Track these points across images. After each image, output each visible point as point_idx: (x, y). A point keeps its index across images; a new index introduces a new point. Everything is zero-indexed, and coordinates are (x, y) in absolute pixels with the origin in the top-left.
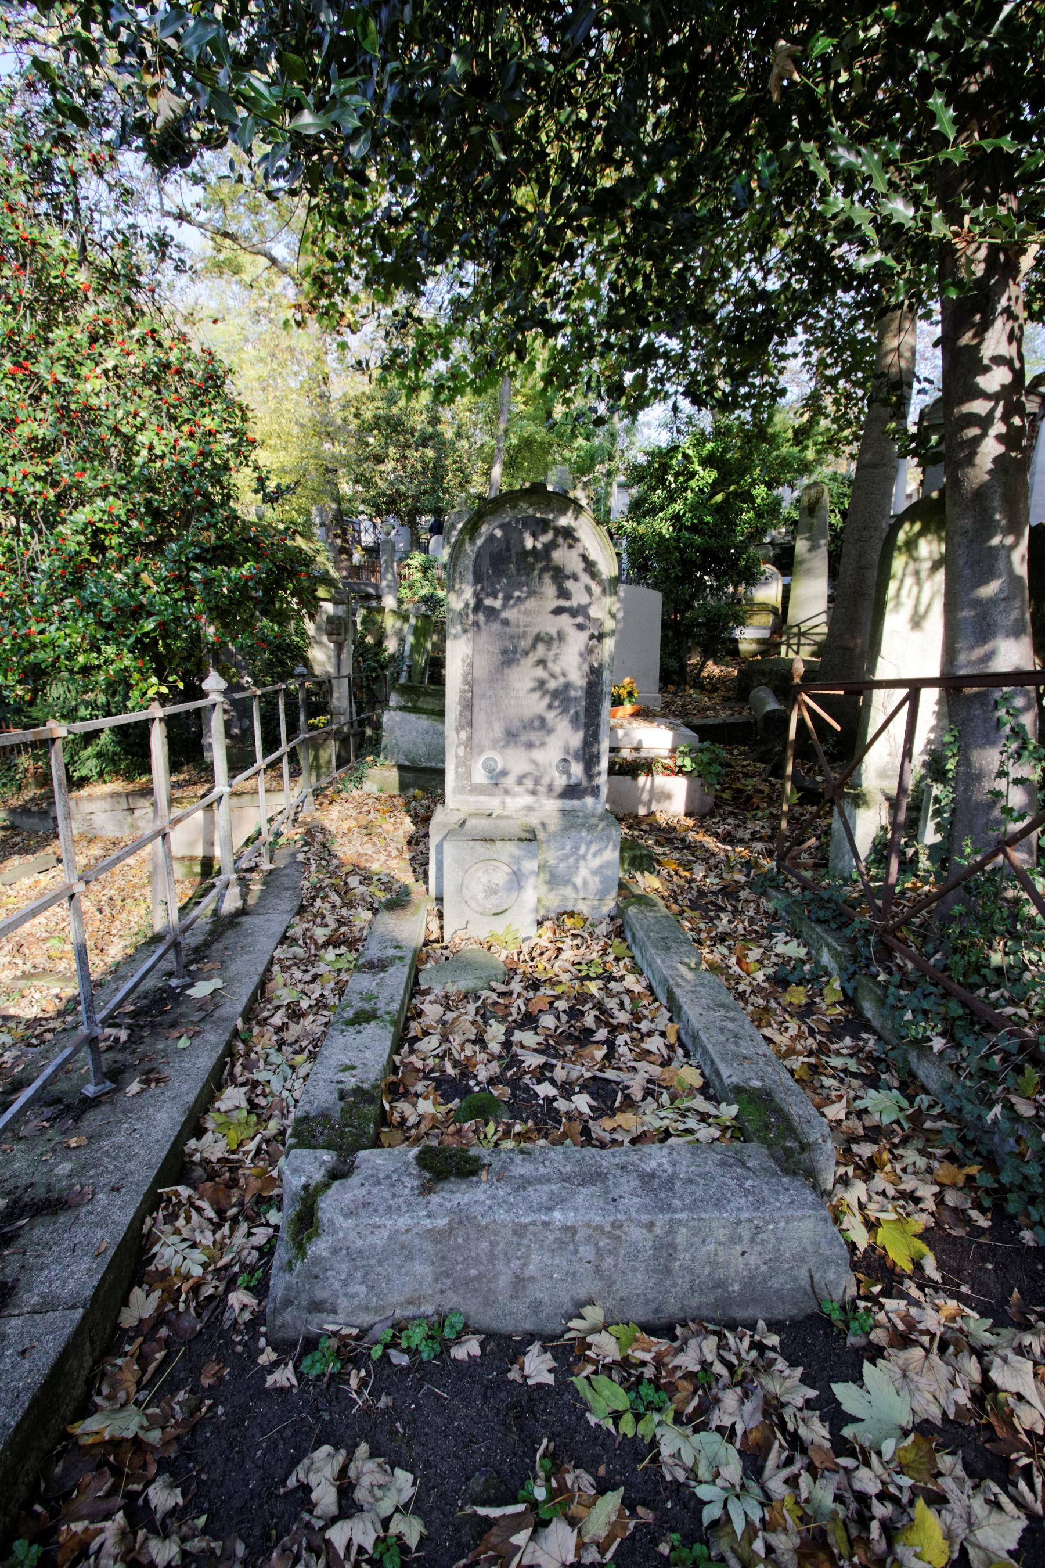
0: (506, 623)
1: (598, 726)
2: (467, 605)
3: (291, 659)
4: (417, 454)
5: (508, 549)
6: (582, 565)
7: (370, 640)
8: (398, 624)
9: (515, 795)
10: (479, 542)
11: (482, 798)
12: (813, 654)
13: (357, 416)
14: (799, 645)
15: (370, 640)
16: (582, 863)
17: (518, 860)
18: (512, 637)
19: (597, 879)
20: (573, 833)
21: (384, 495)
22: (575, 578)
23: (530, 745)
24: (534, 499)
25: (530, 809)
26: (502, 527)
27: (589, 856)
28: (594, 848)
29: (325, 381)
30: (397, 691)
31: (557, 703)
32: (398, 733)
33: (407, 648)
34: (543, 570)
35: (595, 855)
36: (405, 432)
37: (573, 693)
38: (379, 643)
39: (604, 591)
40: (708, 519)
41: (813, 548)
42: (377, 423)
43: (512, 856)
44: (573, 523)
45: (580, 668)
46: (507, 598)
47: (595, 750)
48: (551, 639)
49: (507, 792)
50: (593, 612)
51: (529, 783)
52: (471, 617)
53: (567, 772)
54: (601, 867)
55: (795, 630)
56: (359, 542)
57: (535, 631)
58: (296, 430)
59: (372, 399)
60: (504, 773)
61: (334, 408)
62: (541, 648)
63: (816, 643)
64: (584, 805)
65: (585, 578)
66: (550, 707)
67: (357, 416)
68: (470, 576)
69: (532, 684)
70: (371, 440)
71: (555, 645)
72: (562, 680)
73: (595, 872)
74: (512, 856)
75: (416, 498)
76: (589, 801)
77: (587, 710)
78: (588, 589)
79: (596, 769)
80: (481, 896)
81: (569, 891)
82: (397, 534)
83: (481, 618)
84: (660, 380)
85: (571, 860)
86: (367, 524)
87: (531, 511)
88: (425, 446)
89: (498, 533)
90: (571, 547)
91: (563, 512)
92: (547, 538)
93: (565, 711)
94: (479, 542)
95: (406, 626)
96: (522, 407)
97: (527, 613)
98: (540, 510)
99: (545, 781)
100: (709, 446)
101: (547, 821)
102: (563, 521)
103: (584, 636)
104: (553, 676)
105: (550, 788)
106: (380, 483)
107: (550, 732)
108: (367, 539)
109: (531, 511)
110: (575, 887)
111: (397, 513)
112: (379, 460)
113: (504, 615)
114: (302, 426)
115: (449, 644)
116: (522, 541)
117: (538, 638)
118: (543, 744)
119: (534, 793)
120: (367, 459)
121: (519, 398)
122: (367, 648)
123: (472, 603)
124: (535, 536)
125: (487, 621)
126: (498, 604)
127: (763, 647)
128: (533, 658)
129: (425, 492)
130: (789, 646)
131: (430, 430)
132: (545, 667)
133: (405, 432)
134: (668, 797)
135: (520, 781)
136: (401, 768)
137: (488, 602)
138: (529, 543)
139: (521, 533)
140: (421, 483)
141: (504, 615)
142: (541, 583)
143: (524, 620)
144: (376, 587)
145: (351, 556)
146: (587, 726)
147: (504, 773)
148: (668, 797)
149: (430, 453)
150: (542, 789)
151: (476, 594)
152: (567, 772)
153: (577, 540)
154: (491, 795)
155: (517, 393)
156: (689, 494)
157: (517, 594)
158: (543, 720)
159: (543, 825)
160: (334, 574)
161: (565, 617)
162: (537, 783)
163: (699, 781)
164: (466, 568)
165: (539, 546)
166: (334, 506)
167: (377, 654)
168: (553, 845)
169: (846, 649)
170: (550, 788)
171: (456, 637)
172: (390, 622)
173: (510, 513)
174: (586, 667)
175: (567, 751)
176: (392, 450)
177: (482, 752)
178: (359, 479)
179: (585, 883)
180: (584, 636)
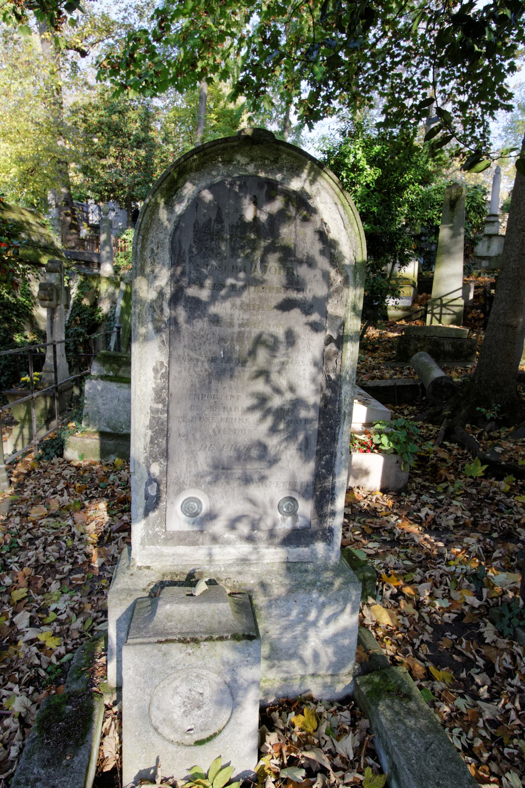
0: (216, 320)
1: (333, 455)
2: (161, 294)
3: (17, 316)
4: (133, 154)
5: (219, 220)
6: (319, 246)
7: (86, 302)
8: (111, 289)
9: (228, 543)
10: (179, 209)
11: (182, 549)
12: (453, 322)
13: (85, 121)
14: (441, 314)
15: (86, 302)
16: (311, 633)
17: (233, 669)
18: (222, 340)
19: (330, 650)
20: (301, 595)
21: (106, 184)
22: (311, 263)
23: (247, 480)
24: (257, 152)
25: (244, 561)
26: (211, 188)
27: (321, 623)
28: (328, 612)
29: (59, 90)
30: (99, 360)
31: (282, 426)
32: (100, 401)
33: (118, 310)
34: (268, 250)
35: (328, 622)
36: (124, 135)
37: (303, 414)
38: (95, 304)
39: (346, 282)
40: (375, 209)
41: (454, 236)
42: (99, 128)
43: (225, 663)
44: (308, 188)
45: (314, 380)
46: (218, 286)
47: (328, 484)
48: (276, 339)
49: (215, 539)
50: (332, 308)
51: (244, 528)
52: (167, 311)
53: (293, 513)
54: (336, 635)
55: (439, 302)
56: (87, 220)
57: (255, 332)
58: (31, 127)
59: (97, 108)
60: (211, 516)
61: (66, 114)
62: (262, 354)
63: (455, 313)
64: (314, 553)
65: (323, 263)
66: (273, 430)
67: (85, 121)
68: (166, 255)
69: (250, 402)
70: (96, 140)
71: (282, 349)
72: (289, 396)
73: (327, 642)
74: (225, 663)
75: (132, 188)
76: (320, 547)
77: (319, 433)
78: (326, 276)
79: (330, 508)
80: (177, 713)
81: (294, 665)
82: (117, 215)
83: (182, 313)
84: (328, 98)
85: (299, 629)
86: (93, 207)
87: (251, 169)
88: (139, 147)
89: (207, 196)
90: (305, 219)
91: (296, 172)
92: (277, 205)
93: (291, 437)
94: (179, 209)
95: (117, 291)
96: (215, 122)
97: (245, 307)
98: (263, 167)
99: (268, 523)
100: (377, 148)
101: (268, 580)
102: (295, 185)
103: (319, 339)
104: (278, 391)
105: (272, 534)
106: (102, 174)
107: (274, 462)
108: (94, 218)
109: (251, 169)
110: (302, 661)
111: (116, 198)
112: (102, 156)
113: (213, 309)
114: (37, 124)
115: (135, 348)
116: (239, 211)
117: (259, 341)
118: (263, 479)
119: (250, 539)
120: (93, 155)
121: (213, 116)
122: (84, 309)
123: (168, 292)
124: (256, 202)
125: (189, 320)
126: (204, 294)
127: (407, 313)
128: (251, 369)
129: (138, 184)
130: (433, 315)
131: (143, 135)
132: (268, 380)
133: (124, 135)
134: (366, 473)
135: (232, 525)
136: (103, 435)
137: (192, 291)
138: (249, 214)
139: (238, 199)
140: (135, 177)
141: (213, 309)
142: (264, 269)
143: (239, 316)
144: (98, 255)
145: (79, 231)
146: (319, 455)
147: (211, 516)
148: (366, 473)
149: (143, 153)
150: (262, 535)
151: (174, 279)
152: (293, 513)
153: (314, 211)
154: (194, 543)
155: (211, 111)
156: (358, 188)
157: (230, 281)
158: (263, 447)
159: (263, 585)
160: (59, 244)
161: (296, 313)
162: (255, 526)
163: (395, 458)
164: (160, 245)
165: (263, 217)
166: (64, 190)
167: (92, 314)
168: (275, 612)
169: (510, 326)
170: (272, 534)
171: (146, 338)
172: (104, 287)
173: (223, 169)
174: (321, 378)
175: (293, 486)
176: (112, 149)
177: (180, 490)
178: (86, 170)
179: (316, 656)
180: (319, 339)
